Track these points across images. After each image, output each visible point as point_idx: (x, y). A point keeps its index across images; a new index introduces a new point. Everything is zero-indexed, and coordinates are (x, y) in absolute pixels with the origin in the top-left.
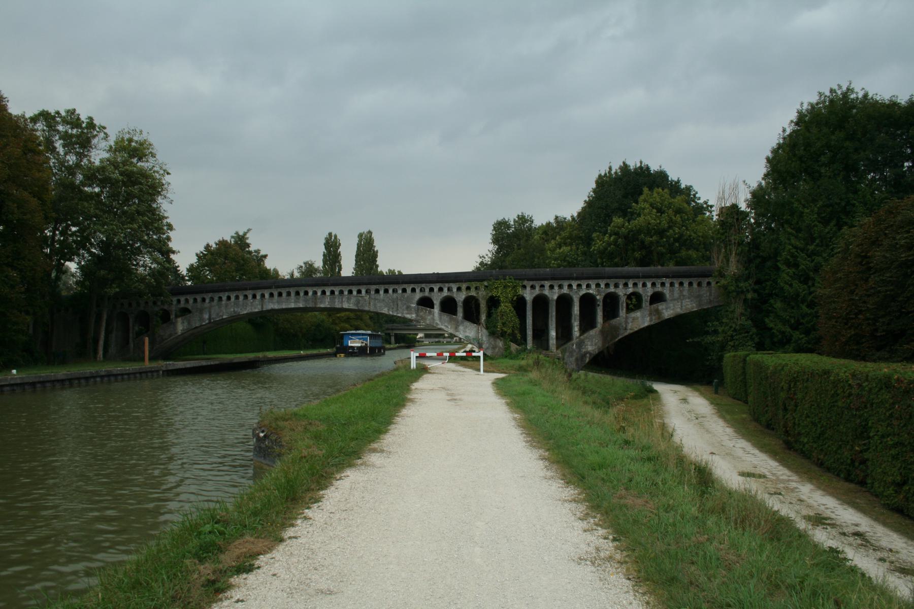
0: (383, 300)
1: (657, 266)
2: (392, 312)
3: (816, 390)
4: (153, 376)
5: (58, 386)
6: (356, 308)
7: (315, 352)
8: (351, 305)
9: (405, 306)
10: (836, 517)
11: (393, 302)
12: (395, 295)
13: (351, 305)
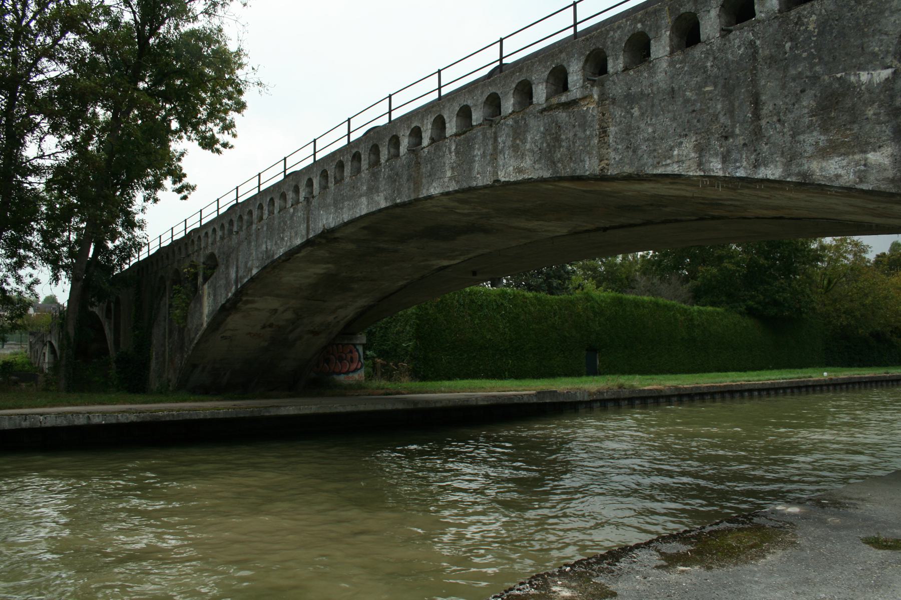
0: (672, 92)
2: (725, 159)
3: (426, 304)
6: (547, 174)
7: (844, 374)
8: (527, 163)
9: (808, 101)
11: (728, 91)
12: (741, 36)
13: (527, 163)
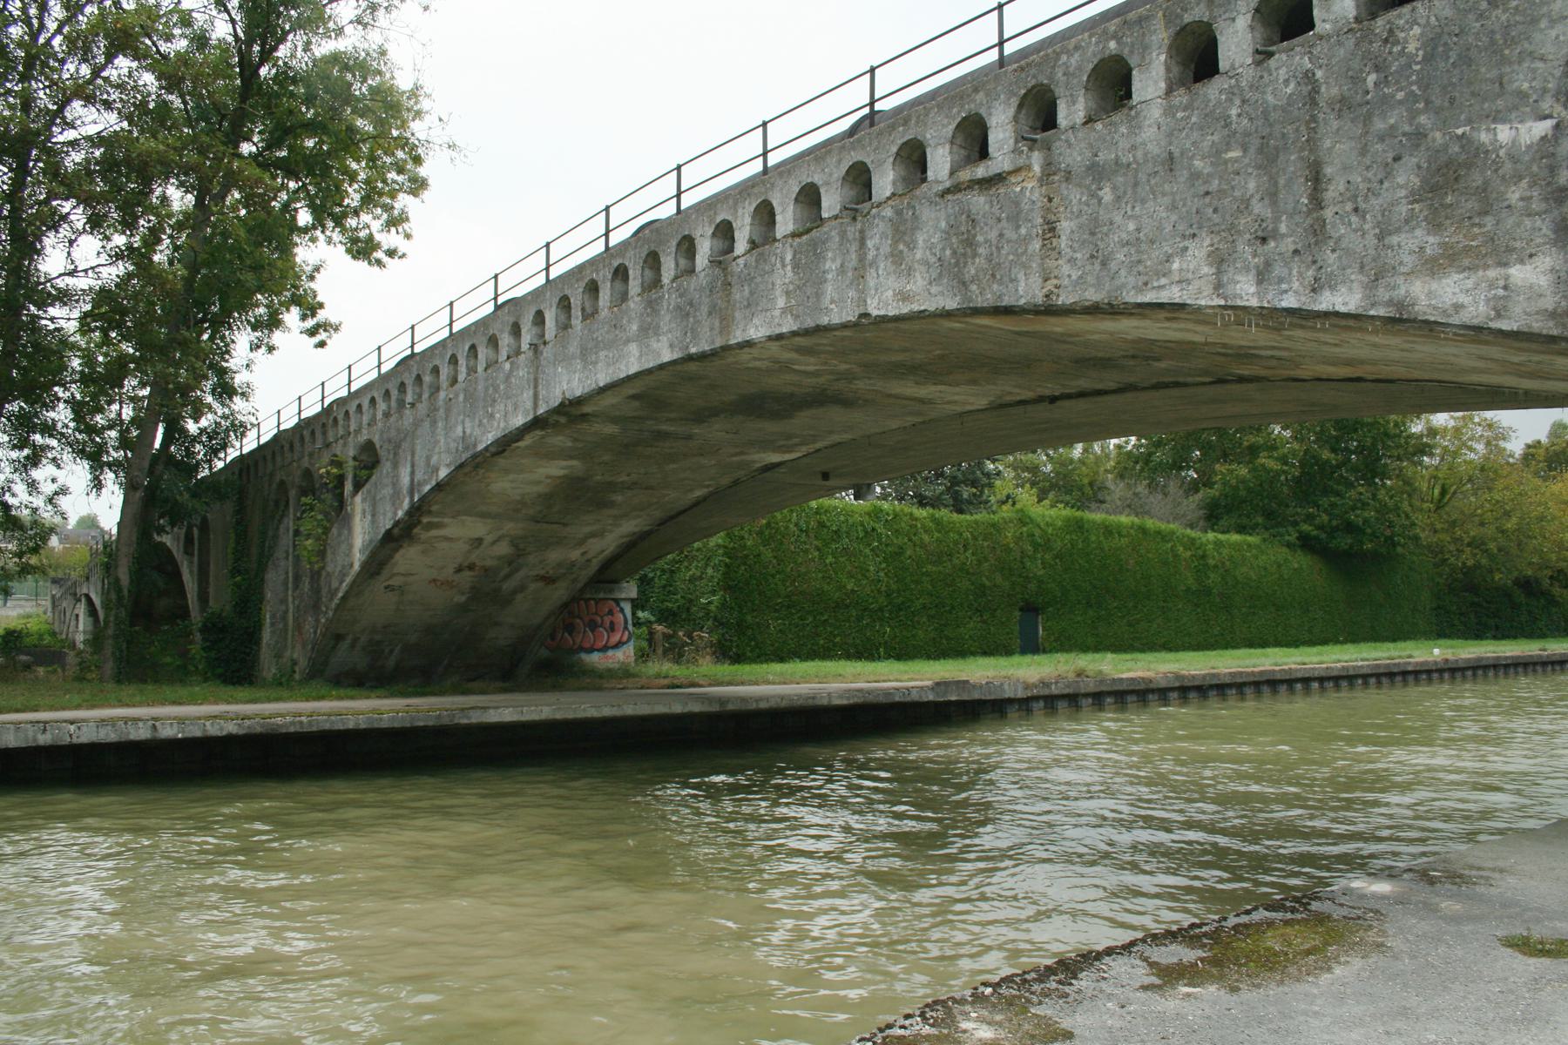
1: (695, 661)
4: (1474, 675)
5: (1411, 678)
6: (951, 304)
8: (918, 283)
9: (1406, 177)
10: (598, 896)
11: (1268, 158)
13: (918, 283)
